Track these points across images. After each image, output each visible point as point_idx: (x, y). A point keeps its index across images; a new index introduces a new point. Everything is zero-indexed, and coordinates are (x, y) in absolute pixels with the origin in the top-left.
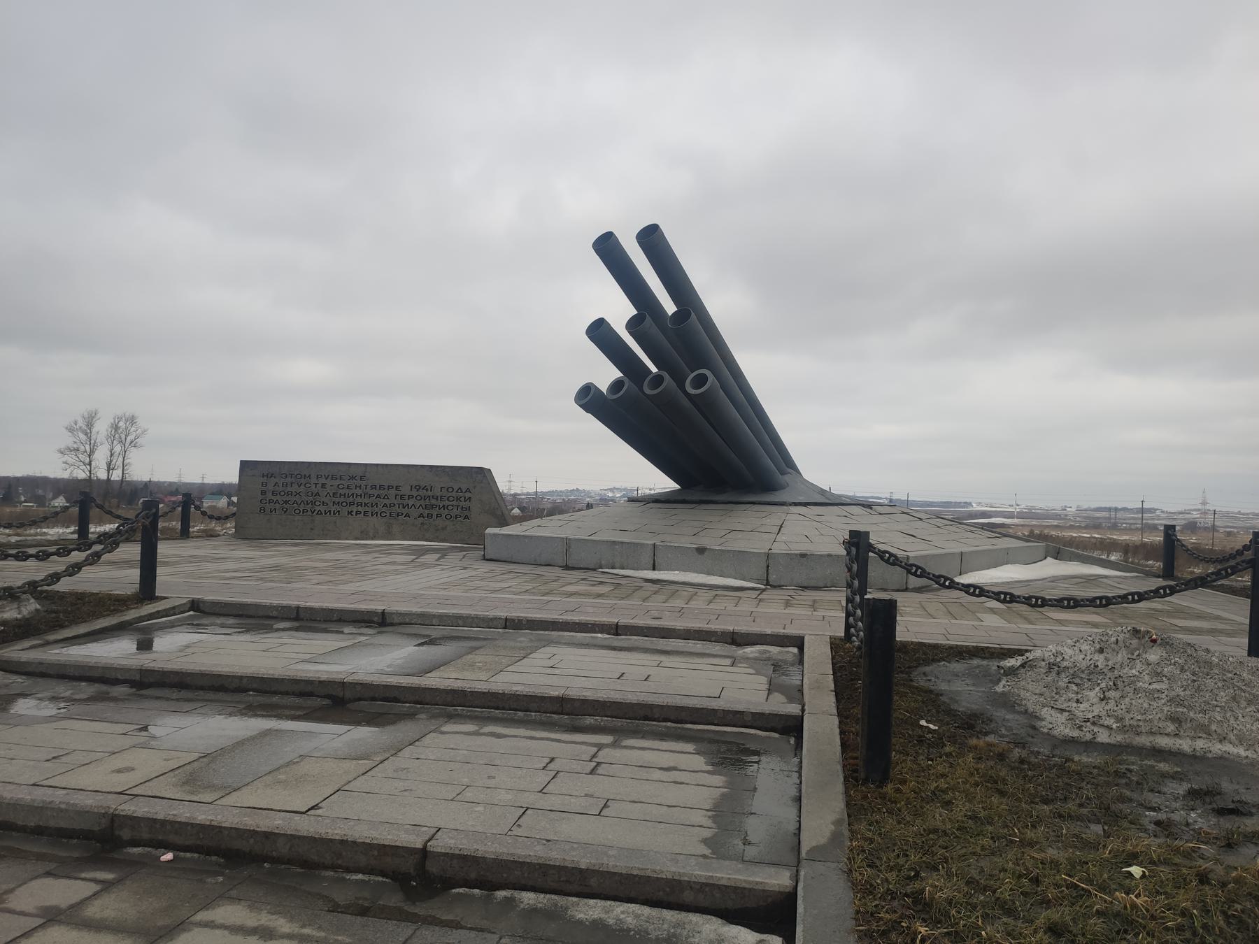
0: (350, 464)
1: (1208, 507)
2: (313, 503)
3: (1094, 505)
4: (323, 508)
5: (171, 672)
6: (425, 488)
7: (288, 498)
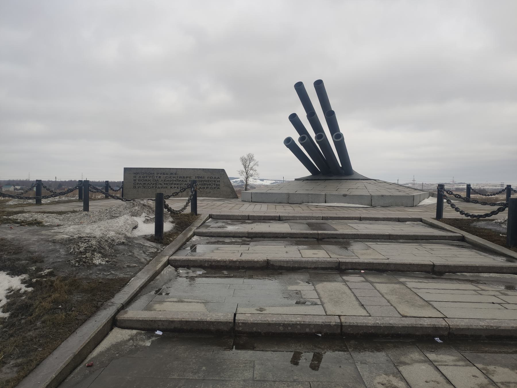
0: (177, 169)
1: (415, 182)
2: (156, 184)
4: (160, 186)
5: (259, 233)
6: (201, 177)
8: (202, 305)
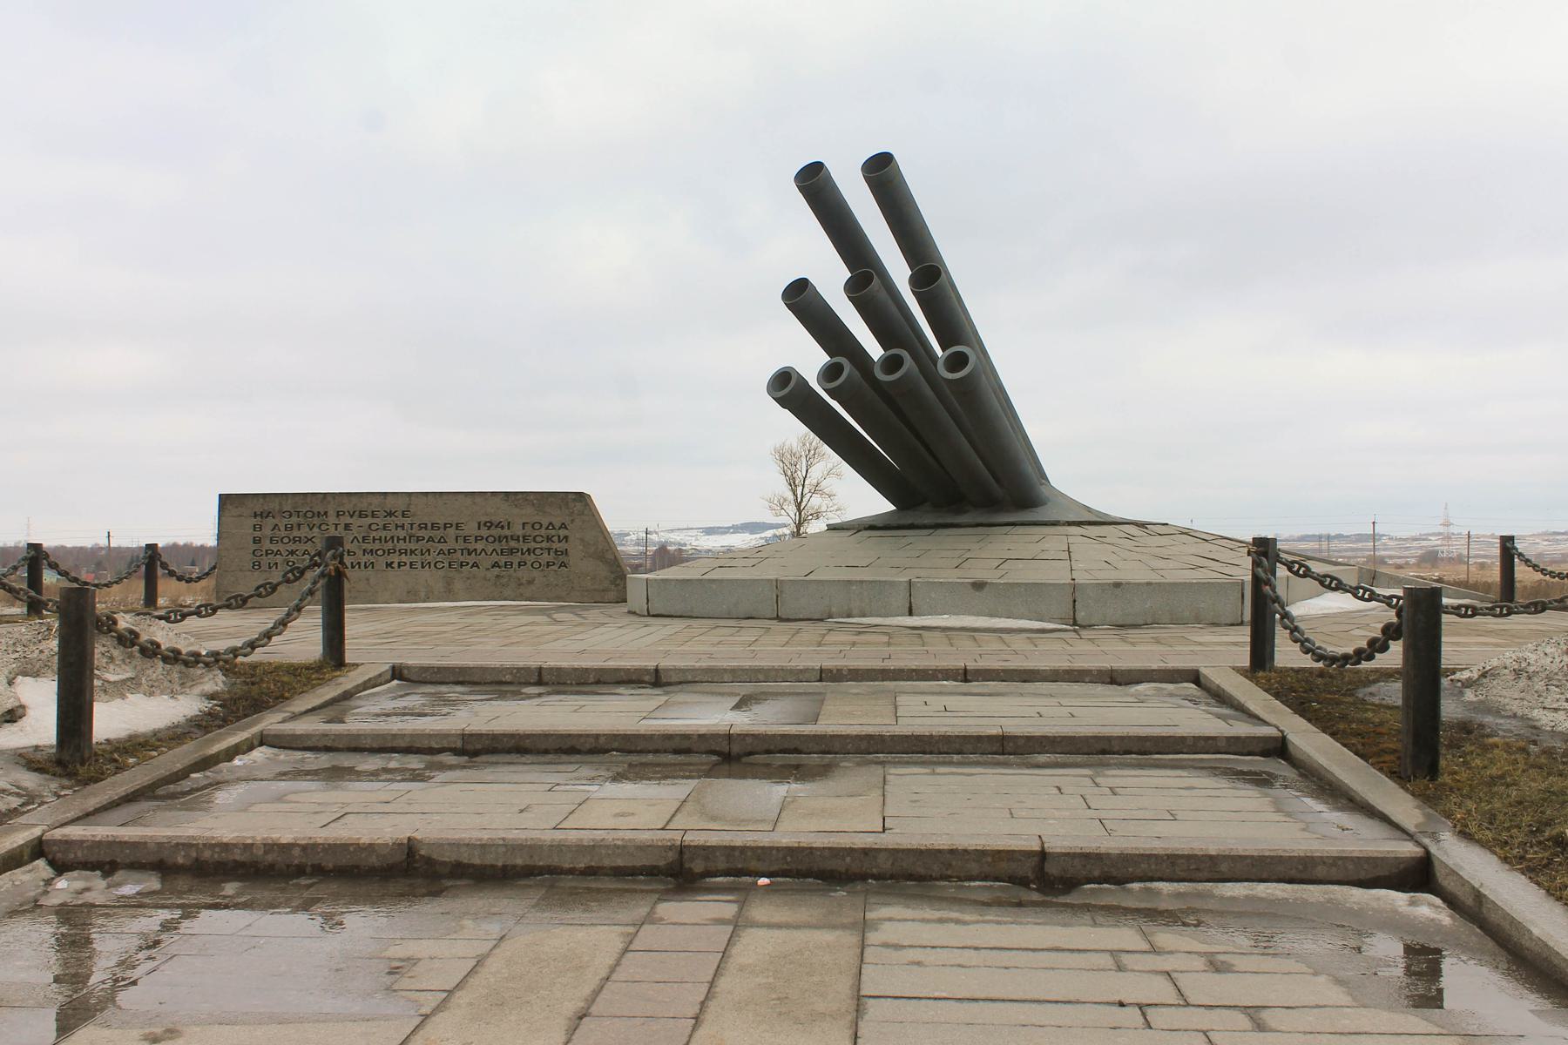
1: (1453, 530)
3: (1297, 533)
5: (504, 735)
6: (499, 525)
7: (294, 547)
8: (1107, 956)
